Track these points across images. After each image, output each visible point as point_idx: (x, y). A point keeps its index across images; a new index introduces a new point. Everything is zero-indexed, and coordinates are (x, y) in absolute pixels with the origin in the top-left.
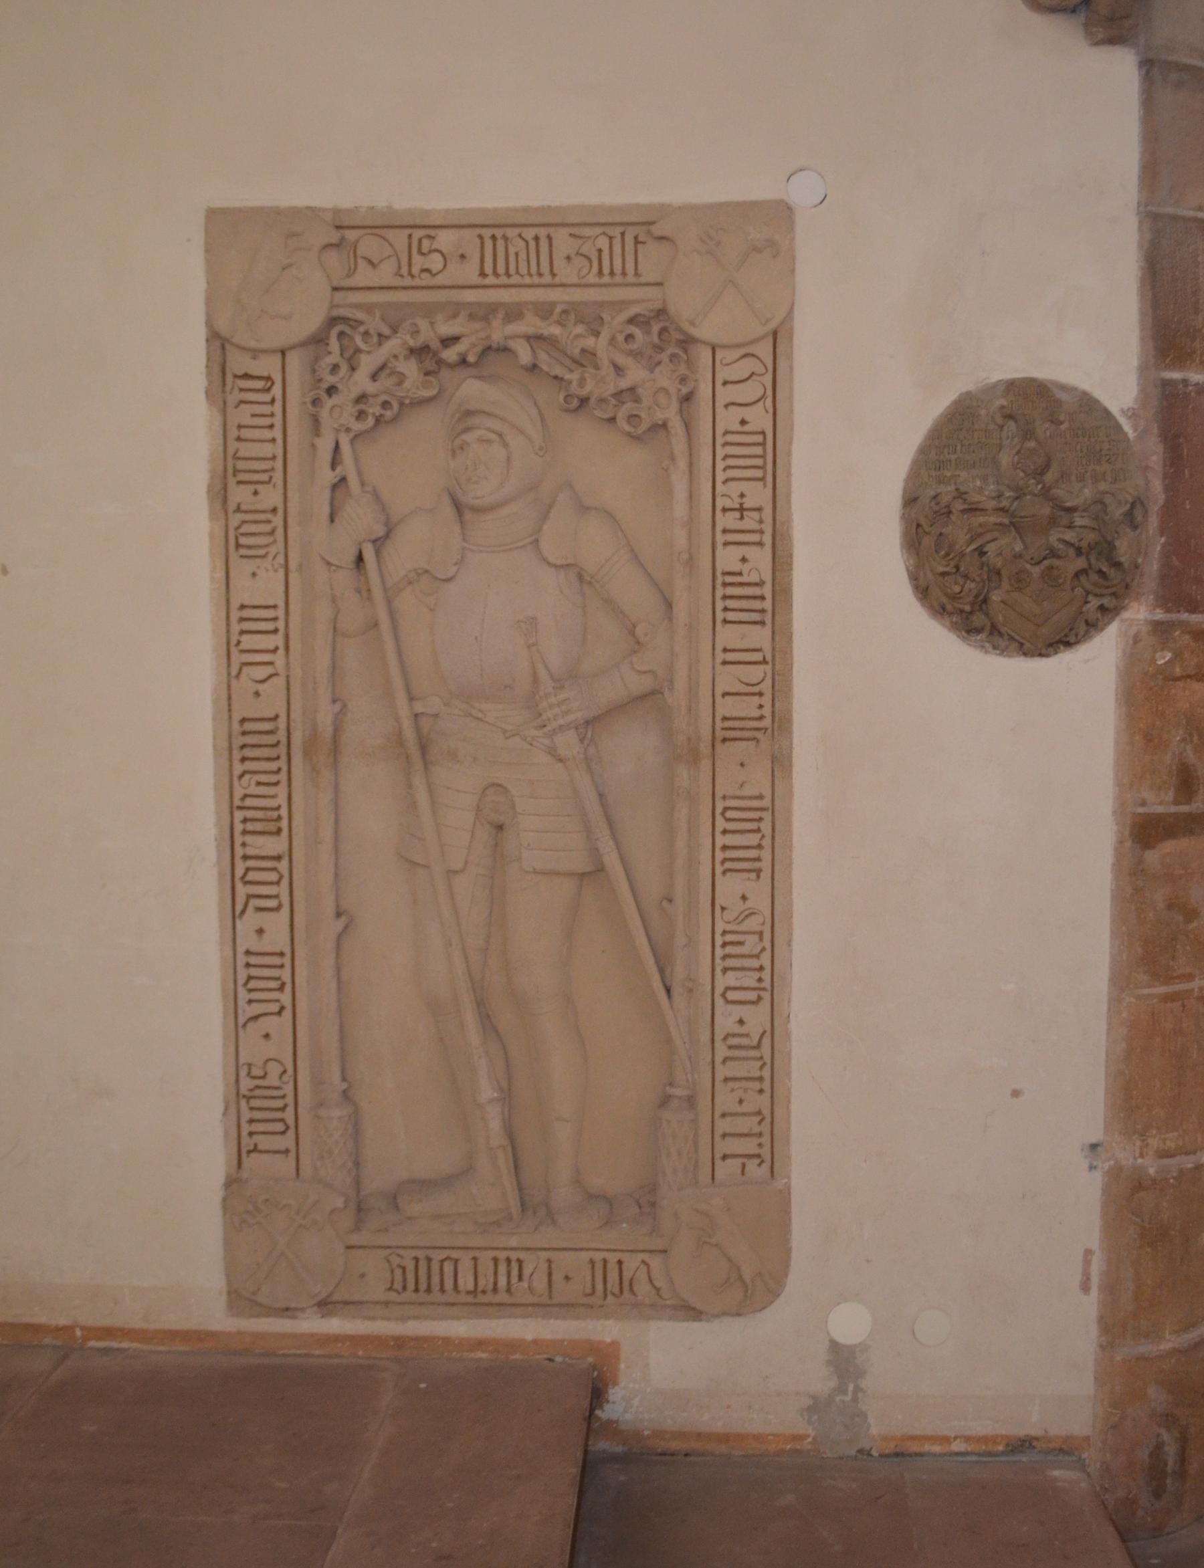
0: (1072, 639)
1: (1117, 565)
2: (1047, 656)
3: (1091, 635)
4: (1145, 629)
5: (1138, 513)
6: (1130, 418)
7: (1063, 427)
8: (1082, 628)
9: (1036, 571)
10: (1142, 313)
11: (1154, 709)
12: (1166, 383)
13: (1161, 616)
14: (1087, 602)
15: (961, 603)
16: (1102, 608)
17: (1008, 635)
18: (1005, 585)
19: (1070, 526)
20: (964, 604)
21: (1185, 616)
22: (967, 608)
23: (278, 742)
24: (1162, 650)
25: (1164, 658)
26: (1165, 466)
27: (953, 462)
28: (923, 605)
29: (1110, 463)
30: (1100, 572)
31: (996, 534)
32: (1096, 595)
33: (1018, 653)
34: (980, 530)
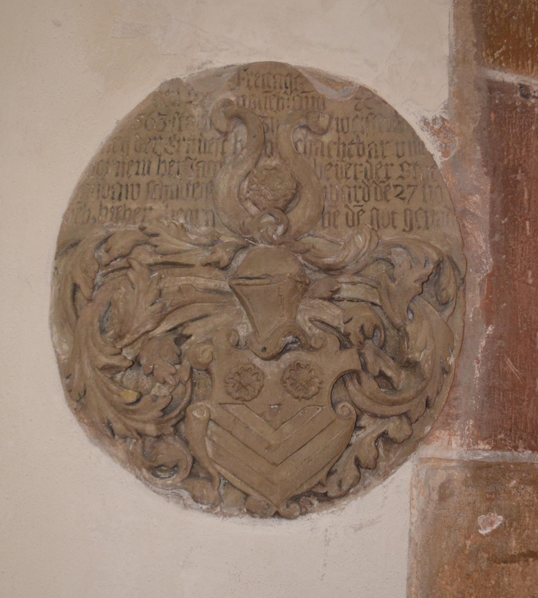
3: (367, 482)
4: (458, 475)
6: (436, 133)
13: (486, 454)
16: (384, 435)
20: (145, 422)
24: (488, 511)
25: (491, 524)
26: (492, 213)
27: (143, 186)
28: (80, 420)
29: (403, 199)
32: (374, 416)
33: (240, 510)
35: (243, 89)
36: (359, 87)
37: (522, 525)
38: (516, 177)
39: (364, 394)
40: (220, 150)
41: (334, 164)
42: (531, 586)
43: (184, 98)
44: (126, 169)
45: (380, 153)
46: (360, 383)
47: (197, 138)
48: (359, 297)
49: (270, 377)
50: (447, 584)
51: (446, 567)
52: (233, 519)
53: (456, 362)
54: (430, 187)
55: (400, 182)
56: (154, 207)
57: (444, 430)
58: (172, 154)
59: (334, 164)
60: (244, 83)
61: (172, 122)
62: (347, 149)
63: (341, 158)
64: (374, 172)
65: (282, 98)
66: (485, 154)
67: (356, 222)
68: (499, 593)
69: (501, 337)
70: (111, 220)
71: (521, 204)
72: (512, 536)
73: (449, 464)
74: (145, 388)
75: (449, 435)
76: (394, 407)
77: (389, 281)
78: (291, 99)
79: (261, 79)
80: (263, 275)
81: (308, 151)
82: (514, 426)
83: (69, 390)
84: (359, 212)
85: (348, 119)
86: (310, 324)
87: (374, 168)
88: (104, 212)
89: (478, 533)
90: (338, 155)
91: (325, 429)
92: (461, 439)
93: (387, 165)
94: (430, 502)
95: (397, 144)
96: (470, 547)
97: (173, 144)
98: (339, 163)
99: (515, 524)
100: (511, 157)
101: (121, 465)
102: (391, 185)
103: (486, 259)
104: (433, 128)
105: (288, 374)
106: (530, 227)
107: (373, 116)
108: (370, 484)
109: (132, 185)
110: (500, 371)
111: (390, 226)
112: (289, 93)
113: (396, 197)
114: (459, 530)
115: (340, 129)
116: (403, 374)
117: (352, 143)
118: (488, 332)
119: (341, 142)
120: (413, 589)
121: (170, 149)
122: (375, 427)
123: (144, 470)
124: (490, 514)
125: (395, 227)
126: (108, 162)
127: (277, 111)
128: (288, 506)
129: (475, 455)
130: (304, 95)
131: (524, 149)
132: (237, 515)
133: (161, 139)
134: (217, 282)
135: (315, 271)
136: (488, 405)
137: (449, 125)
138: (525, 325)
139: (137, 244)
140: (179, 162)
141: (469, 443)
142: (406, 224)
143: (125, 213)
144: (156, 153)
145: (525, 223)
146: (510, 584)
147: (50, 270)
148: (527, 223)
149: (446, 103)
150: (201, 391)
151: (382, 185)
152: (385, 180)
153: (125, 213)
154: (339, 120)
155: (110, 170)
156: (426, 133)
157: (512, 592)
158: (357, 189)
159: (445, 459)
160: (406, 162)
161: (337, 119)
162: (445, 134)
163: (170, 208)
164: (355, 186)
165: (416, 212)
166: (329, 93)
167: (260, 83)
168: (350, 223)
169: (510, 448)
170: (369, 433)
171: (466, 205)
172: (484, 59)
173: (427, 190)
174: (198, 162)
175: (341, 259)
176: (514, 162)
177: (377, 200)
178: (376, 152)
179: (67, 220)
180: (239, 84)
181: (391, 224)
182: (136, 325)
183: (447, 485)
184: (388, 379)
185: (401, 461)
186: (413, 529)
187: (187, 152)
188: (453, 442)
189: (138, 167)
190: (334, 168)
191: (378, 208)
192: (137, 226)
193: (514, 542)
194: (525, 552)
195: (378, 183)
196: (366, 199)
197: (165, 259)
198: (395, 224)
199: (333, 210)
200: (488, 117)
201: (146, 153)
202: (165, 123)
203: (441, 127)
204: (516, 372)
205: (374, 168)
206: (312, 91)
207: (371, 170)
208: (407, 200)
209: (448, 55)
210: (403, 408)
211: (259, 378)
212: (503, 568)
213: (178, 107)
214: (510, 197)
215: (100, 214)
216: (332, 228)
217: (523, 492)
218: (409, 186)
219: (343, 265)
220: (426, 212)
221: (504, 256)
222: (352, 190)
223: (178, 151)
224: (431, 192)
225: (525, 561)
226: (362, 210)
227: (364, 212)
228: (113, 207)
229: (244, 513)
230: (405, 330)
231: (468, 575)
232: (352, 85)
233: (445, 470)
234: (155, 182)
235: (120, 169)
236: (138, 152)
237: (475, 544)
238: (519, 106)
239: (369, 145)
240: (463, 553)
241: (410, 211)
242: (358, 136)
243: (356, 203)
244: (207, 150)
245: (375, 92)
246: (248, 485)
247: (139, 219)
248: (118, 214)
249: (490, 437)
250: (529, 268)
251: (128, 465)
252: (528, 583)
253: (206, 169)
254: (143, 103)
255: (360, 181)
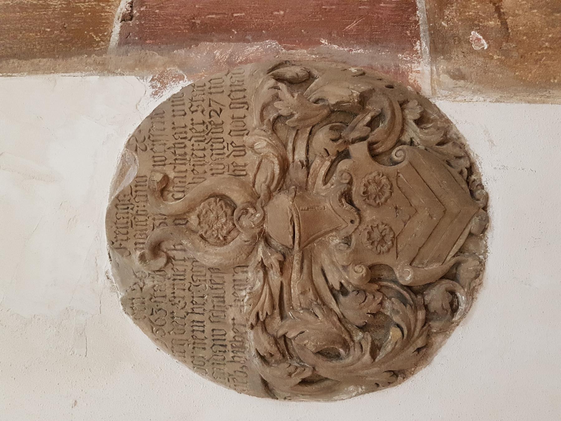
0: (464, 163)
1: (363, 99)
2: (487, 197)
3: (454, 137)
4: (443, 65)
5: (289, 72)
6: (164, 86)
7: (172, 175)
8: (448, 148)
9: (369, 215)
10: (35, 71)
11: (550, 52)
12: (125, 40)
13: (424, 44)
14: (412, 143)
15: (415, 326)
16: (419, 122)
17: (456, 255)
18: (387, 260)
19: (307, 165)
20: (416, 320)
21: (421, 15)
22: (421, 315)
23: (223, 91)
24: (469, 43)
25: (479, 40)
26: (229, 41)
27: (214, 326)
28: (412, 374)
29: (221, 110)
30: (372, 124)
31: (316, 269)
32: (402, 131)
33: (481, 239)
34: (311, 295)
35: (130, 245)
36: (127, 148)
37: (476, 17)
38: (198, 24)
39: (386, 139)
40: (182, 262)
41: (193, 167)
42: (523, 10)
43: (138, 294)
44: (200, 341)
45: (183, 130)
46: (376, 143)
47: (172, 282)
48: (305, 145)
49: (374, 217)
50: (530, 72)
51: (517, 74)
52: (489, 244)
53: (355, 66)
54: (210, 88)
55: (206, 113)
56: (232, 317)
57: (408, 76)
58: (186, 303)
59: (193, 167)
60: (124, 244)
61: (158, 304)
62: (180, 157)
63: (188, 162)
64: (198, 134)
65: (137, 212)
66: (180, 47)
67: (241, 148)
68: (532, 33)
69: (330, 34)
70: (243, 352)
71: (220, 20)
72: (486, 24)
73: (435, 73)
74: (384, 320)
75: (411, 72)
76: (396, 114)
77: (293, 119)
78: (138, 204)
79: (120, 230)
80: (291, 224)
81: (182, 189)
82: (399, 24)
83: (389, 384)
84: (233, 146)
85: (154, 157)
86: (329, 184)
87: (196, 134)
88: (236, 359)
89: (487, 49)
90: (185, 164)
91: (416, 170)
92: (414, 63)
93: (192, 124)
94: (466, 86)
95: (174, 116)
96: (499, 56)
97: (177, 302)
98: (192, 164)
99: (476, 22)
100: (182, 28)
101: (448, 338)
102: (210, 120)
103: (267, 45)
104: (159, 87)
105: (371, 201)
106: (238, 13)
107: (151, 136)
108: (456, 134)
109: (213, 336)
110: (357, 34)
111: (244, 120)
112: (133, 206)
113: (219, 116)
114: (487, 64)
115: (163, 163)
116: (368, 107)
117: (175, 153)
118: (327, 43)
119: (174, 162)
120: (537, 99)
121: (182, 304)
122: (410, 130)
123: (454, 319)
124: (471, 41)
125: (245, 117)
126: (193, 357)
127: (148, 216)
128: (478, 200)
129: (425, 52)
130: (134, 193)
131: (175, 18)
132: (485, 241)
133: (173, 312)
134: (295, 263)
135: (284, 182)
136: (385, 43)
137: (157, 75)
138: (318, 16)
139: (265, 329)
140: (193, 297)
141: (416, 57)
142: (243, 107)
143: (237, 341)
144: (185, 316)
145: (236, 16)
146: (524, 25)
147: (286, 403)
148: (235, 15)
149: (139, 78)
150: (385, 274)
151: (209, 128)
152: (205, 125)
153: (237, 341)
154: (155, 164)
155: (201, 355)
156: (164, 93)
157: (530, 24)
158: (214, 148)
159: (431, 75)
160: (190, 108)
161: (154, 165)
162: (165, 78)
163: (233, 304)
164: (211, 150)
165: (232, 100)
166: (132, 174)
167: (124, 231)
168: (243, 153)
169: (417, 26)
170: (416, 135)
171: (223, 61)
172: (101, 49)
173: (213, 90)
174: (193, 280)
175: (276, 159)
176: (186, 25)
177: (223, 131)
178: (181, 133)
179: (244, 391)
180: (125, 248)
181: (243, 120)
182: (335, 330)
183: (452, 74)
184: (373, 119)
185: (436, 109)
186: (488, 100)
187: (184, 290)
188: (417, 69)
189: (197, 331)
190: (196, 168)
191: (229, 131)
192: (249, 330)
193: (490, 23)
194: (497, 14)
195: (208, 131)
196: (222, 140)
197: (277, 307)
198: (243, 116)
199: (232, 167)
200: (150, 45)
201: (185, 324)
202: (160, 309)
203: (159, 82)
204: (356, 22)
205: (196, 134)
206: (131, 187)
207: (197, 137)
208: (222, 107)
209: (98, 77)
210: (397, 106)
211: (376, 225)
212: (512, 30)
213: (146, 299)
214: (214, 28)
215: (239, 362)
216: (247, 168)
217: (450, 17)
218: (210, 106)
219: (280, 158)
220: (231, 91)
221: (263, 31)
222: (214, 152)
223: (183, 298)
224: (214, 87)
225: (504, 15)
226: (231, 144)
227: (233, 142)
228: (233, 352)
229: (484, 236)
230: (334, 105)
231: (522, 57)
232: (125, 154)
233: (439, 75)
234: (210, 317)
235: (200, 346)
236: (185, 332)
237: (496, 51)
238: (140, 22)
239: (176, 139)
240: (504, 60)
241: (231, 104)
242: (169, 149)
243: (226, 149)
244: (182, 273)
245: (131, 136)
246: (462, 233)
247: (242, 329)
248: (239, 348)
249: (410, 41)
250: (272, 13)
251: (448, 333)
252: (521, 12)
253: (199, 274)
254: (143, 329)
255: (207, 146)
